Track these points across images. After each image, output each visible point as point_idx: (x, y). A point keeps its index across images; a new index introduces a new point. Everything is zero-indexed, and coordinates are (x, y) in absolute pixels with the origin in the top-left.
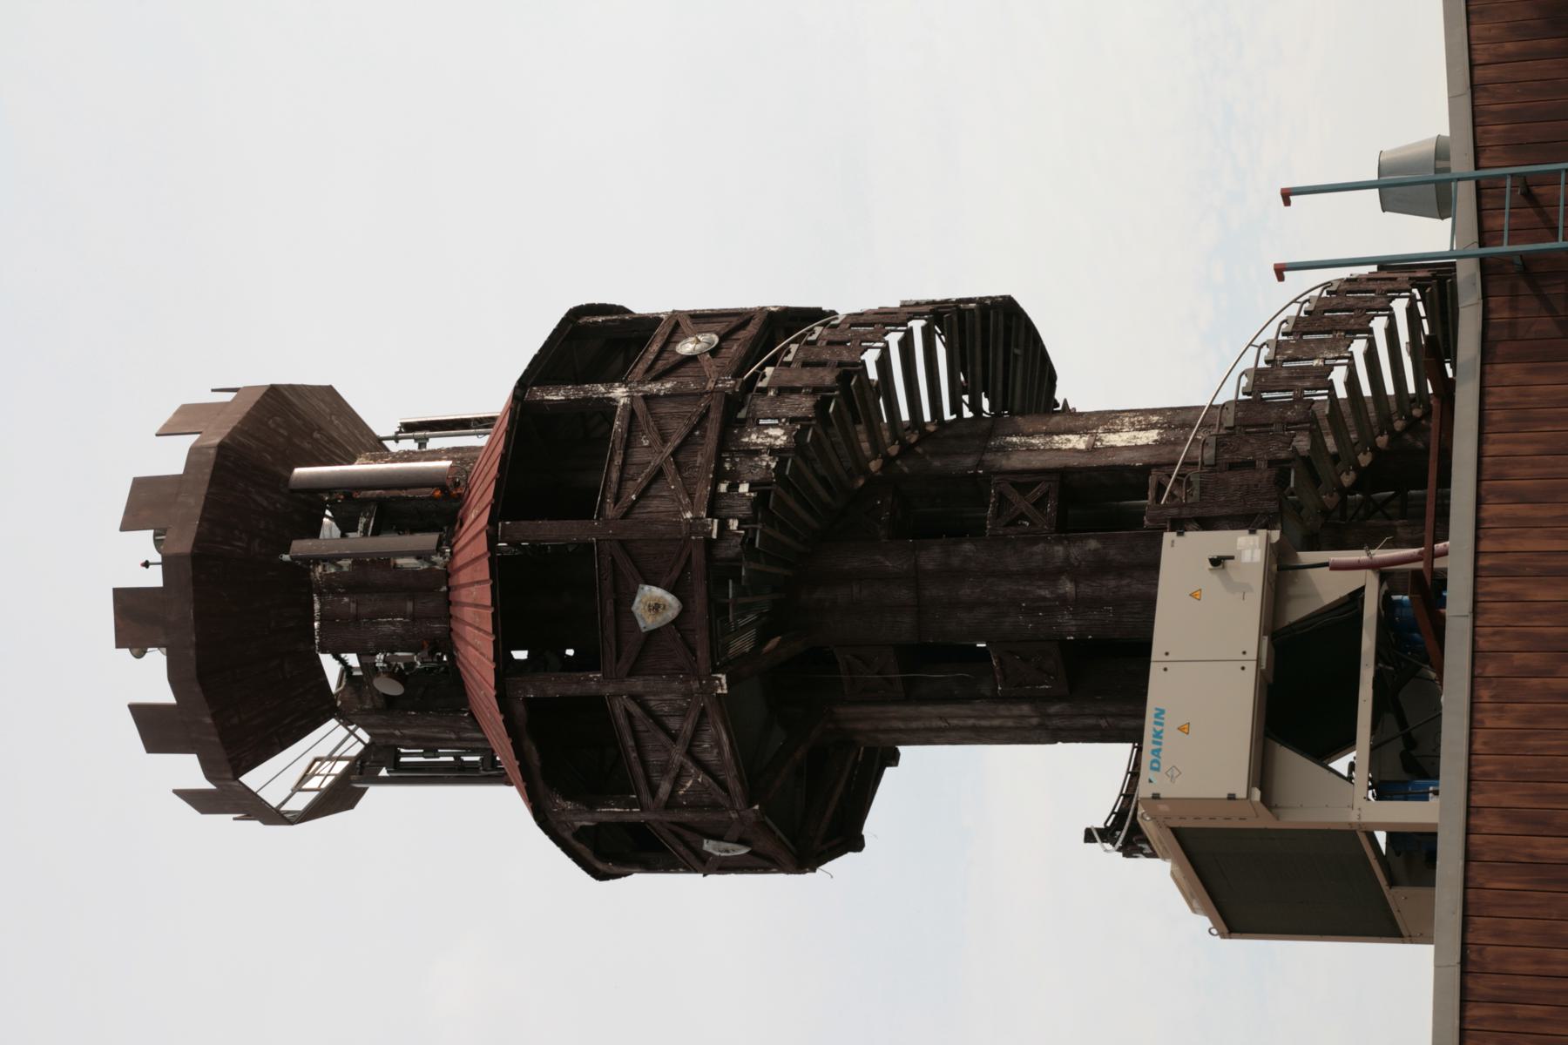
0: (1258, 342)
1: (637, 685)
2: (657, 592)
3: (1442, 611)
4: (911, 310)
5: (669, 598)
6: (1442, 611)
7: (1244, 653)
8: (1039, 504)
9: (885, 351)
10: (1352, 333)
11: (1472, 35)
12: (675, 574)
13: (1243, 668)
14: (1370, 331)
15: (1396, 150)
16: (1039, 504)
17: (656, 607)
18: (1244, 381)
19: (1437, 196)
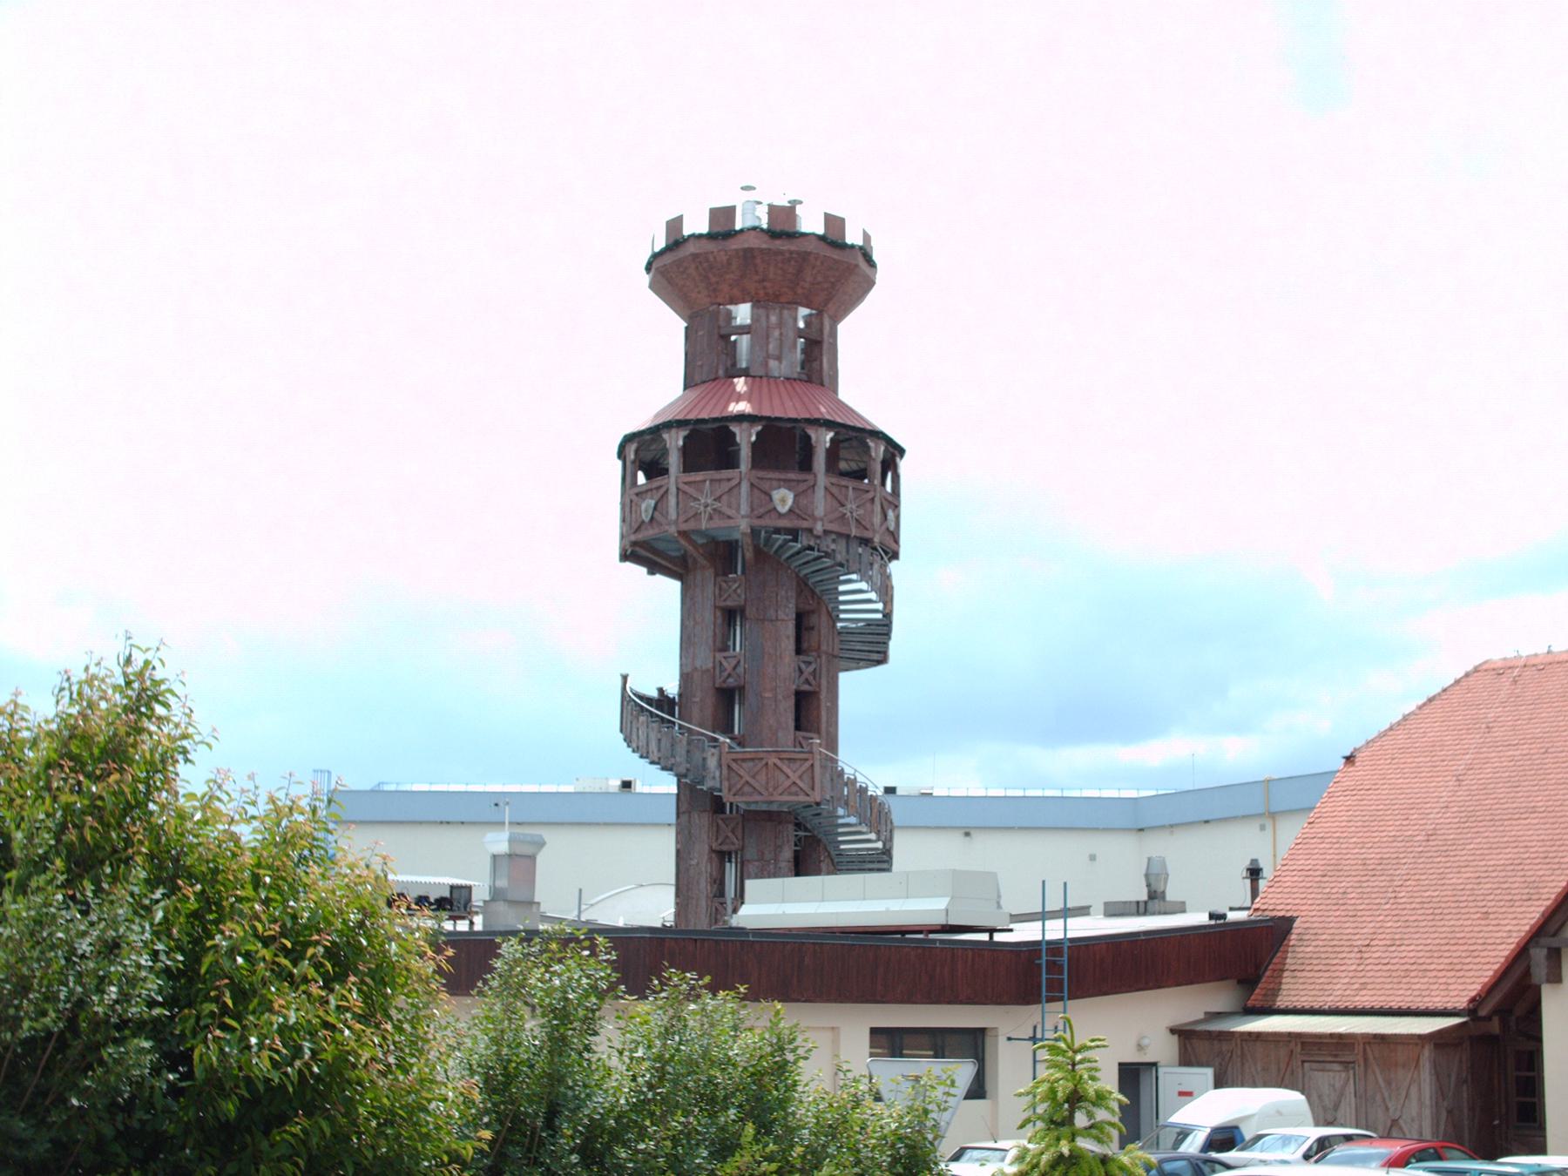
0: (857, 774)
1: (745, 487)
2: (790, 502)
3: (144, 1036)
4: (888, 615)
5: (787, 508)
6: (144, 1036)
7: (1093, 858)
8: (807, 682)
9: (875, 602)
10: (860, 816)
11: (1068, 928)
12: (797, 511)
13: (1093, 858)
14: (860, 824)
15: (1229, 1122)
16: (807, 682)
17: (783, 501)
18: (864, 785)
19: (854, 900)
